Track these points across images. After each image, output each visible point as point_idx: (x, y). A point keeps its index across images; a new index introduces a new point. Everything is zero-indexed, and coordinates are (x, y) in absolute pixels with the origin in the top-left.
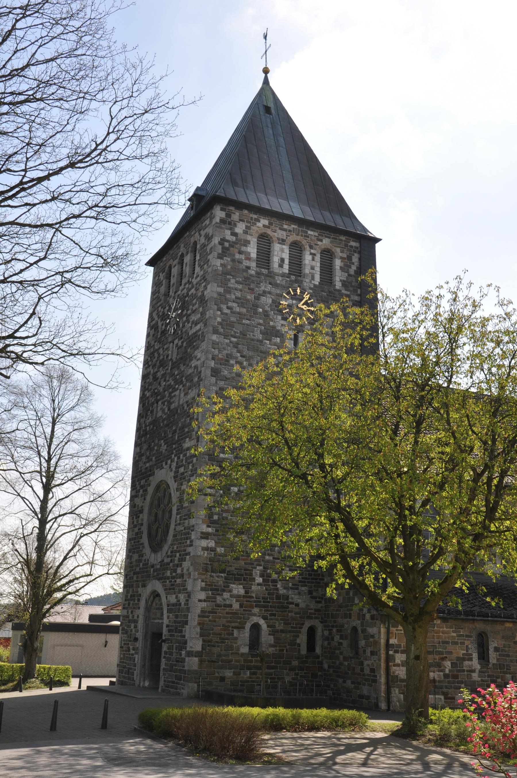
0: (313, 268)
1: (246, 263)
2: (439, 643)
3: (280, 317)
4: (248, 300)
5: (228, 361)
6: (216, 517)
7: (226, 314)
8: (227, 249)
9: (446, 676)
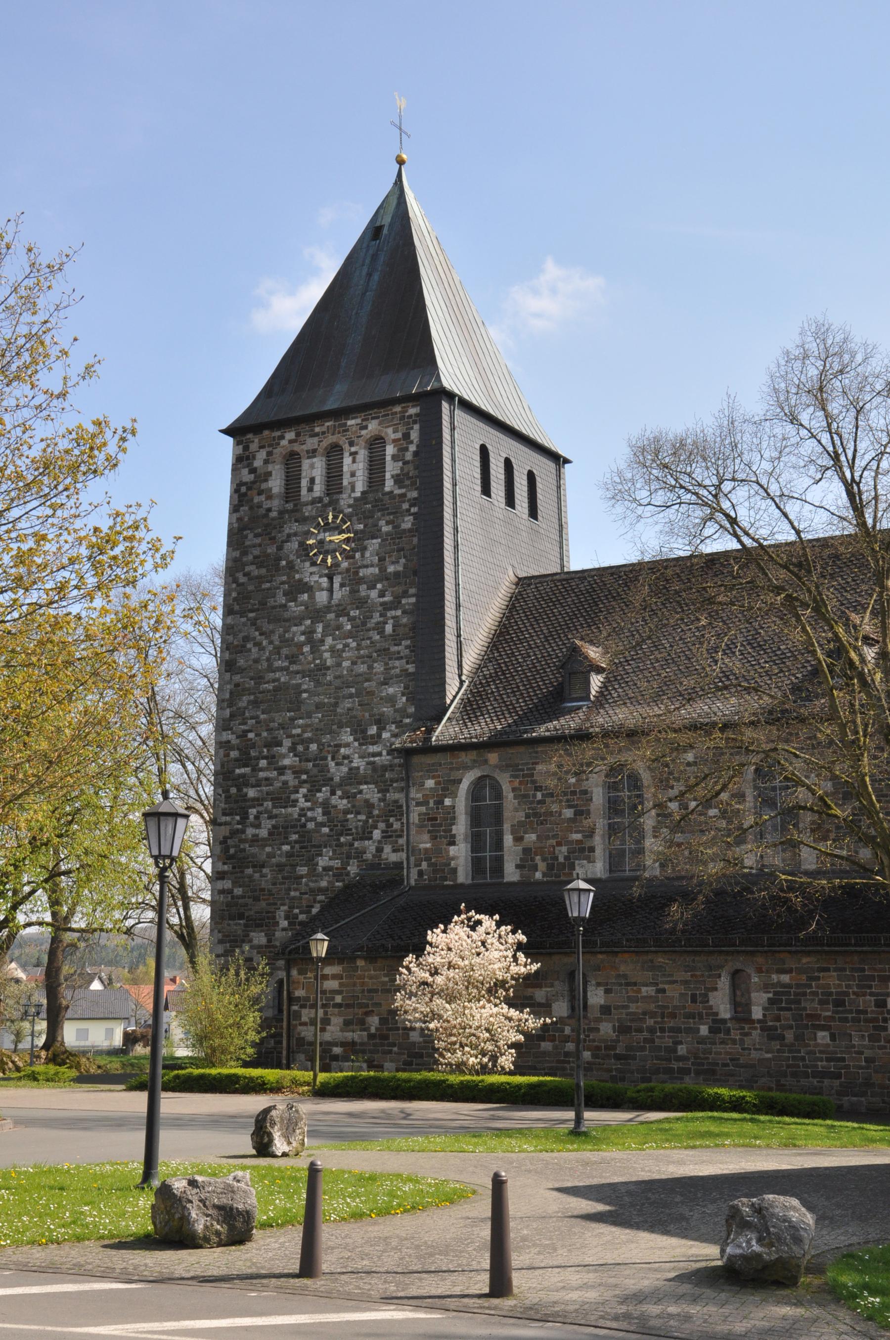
0: (353, 474)
1: (267, 505)
2: (363, 991)
3: (307, 564)
4: (269, 555)
5: (244, 646)
6: (232, 851)
7: (243, 584)
8: (245, 494)
9: (371, 1036)
